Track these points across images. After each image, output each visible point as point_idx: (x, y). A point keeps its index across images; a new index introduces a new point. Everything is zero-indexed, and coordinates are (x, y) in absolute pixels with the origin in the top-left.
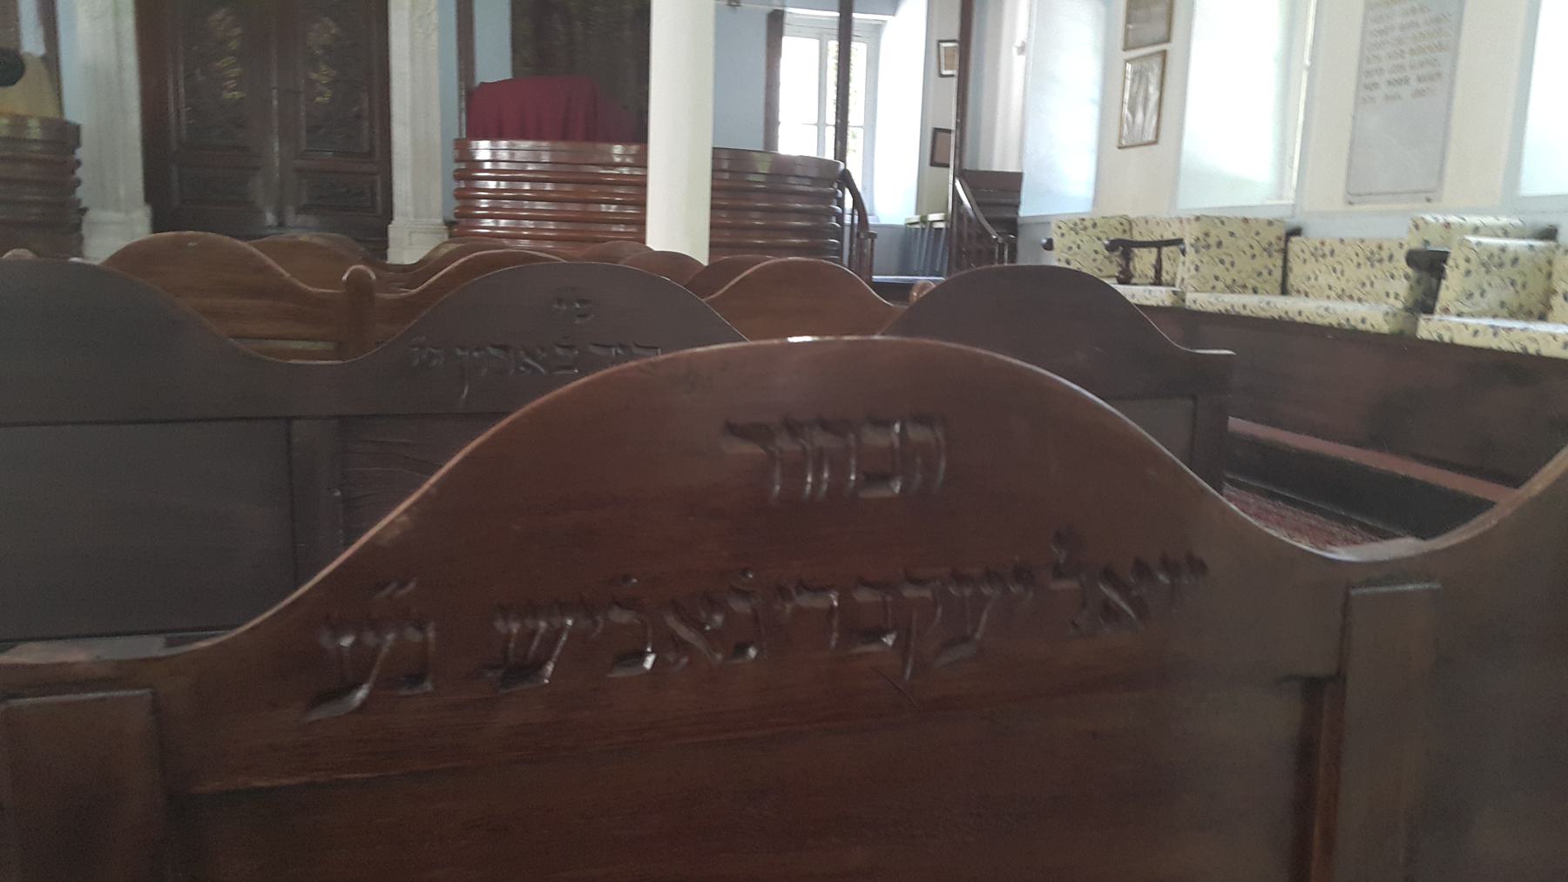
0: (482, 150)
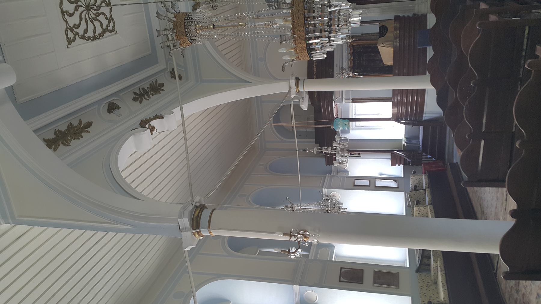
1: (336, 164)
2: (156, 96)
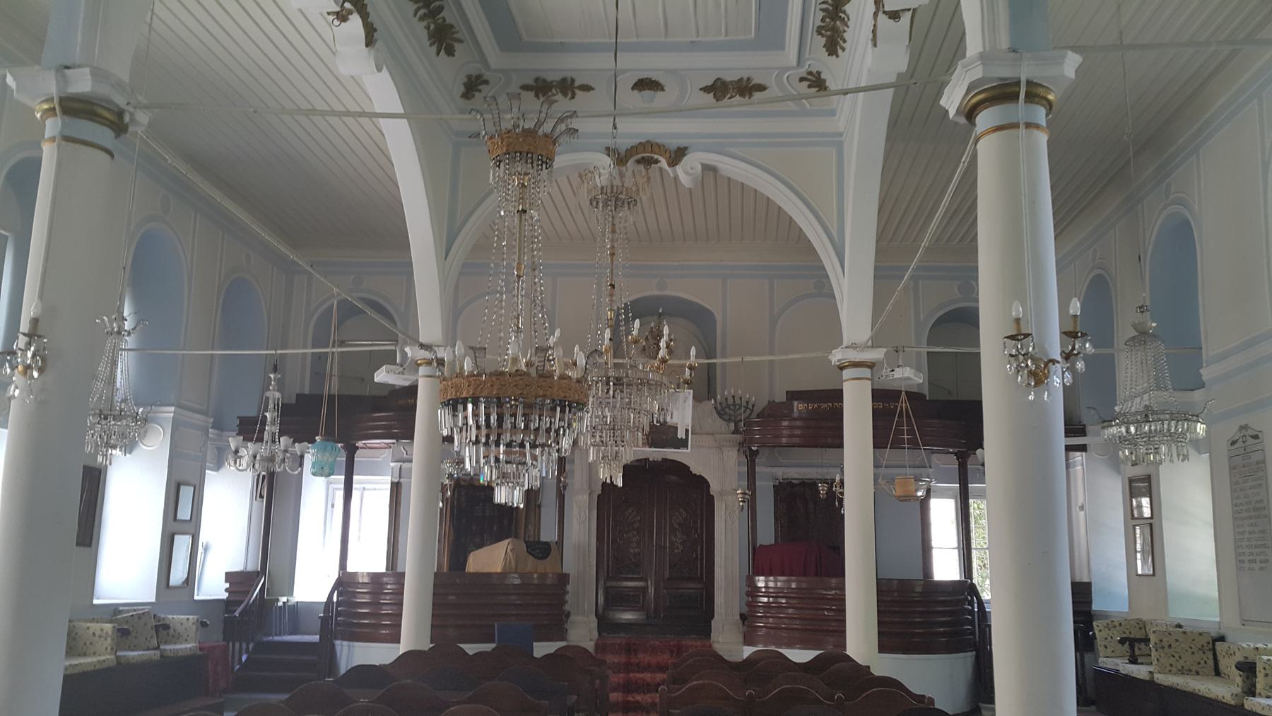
0: (761, 582)
1: (233, 443)
2: (424, 34)
